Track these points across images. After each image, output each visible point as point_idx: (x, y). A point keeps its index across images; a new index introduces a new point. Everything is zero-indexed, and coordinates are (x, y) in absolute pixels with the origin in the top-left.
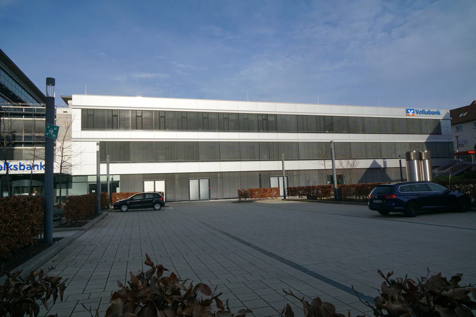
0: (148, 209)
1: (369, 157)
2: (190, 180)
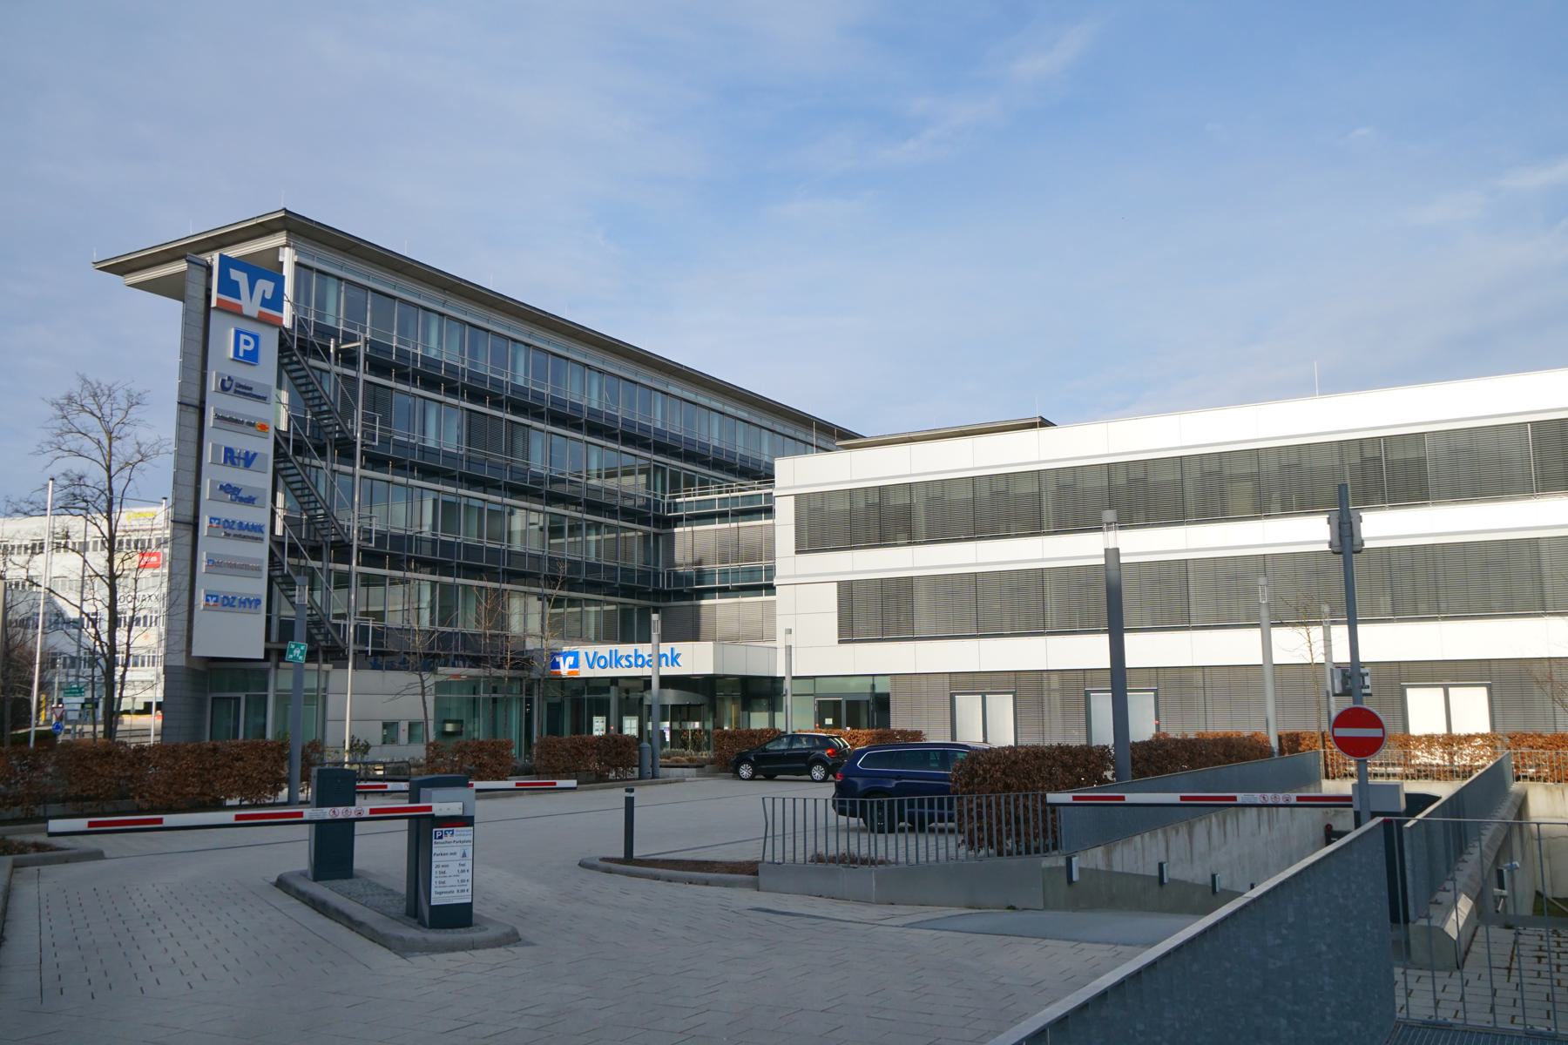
0: (800, 777)
1: (858, 636)
2: (957, 697)
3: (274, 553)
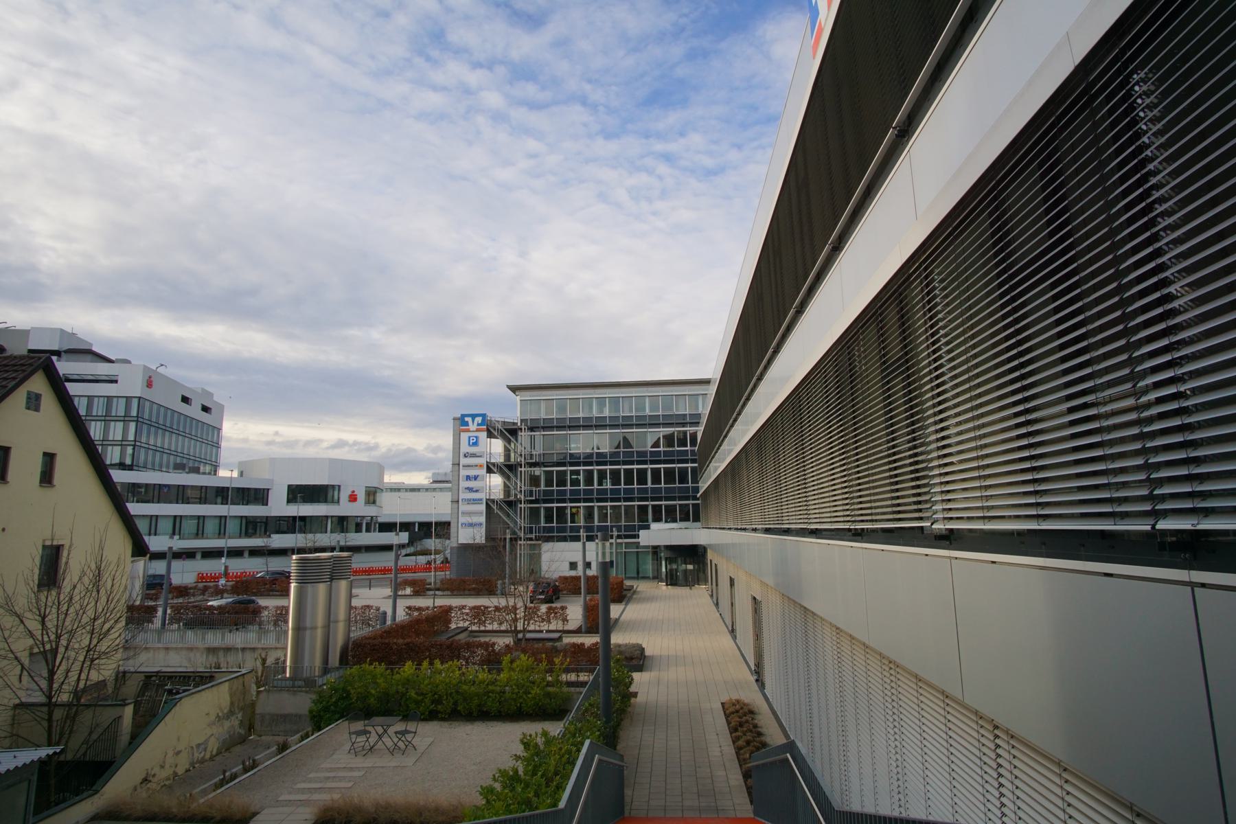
3: (490, 506)
